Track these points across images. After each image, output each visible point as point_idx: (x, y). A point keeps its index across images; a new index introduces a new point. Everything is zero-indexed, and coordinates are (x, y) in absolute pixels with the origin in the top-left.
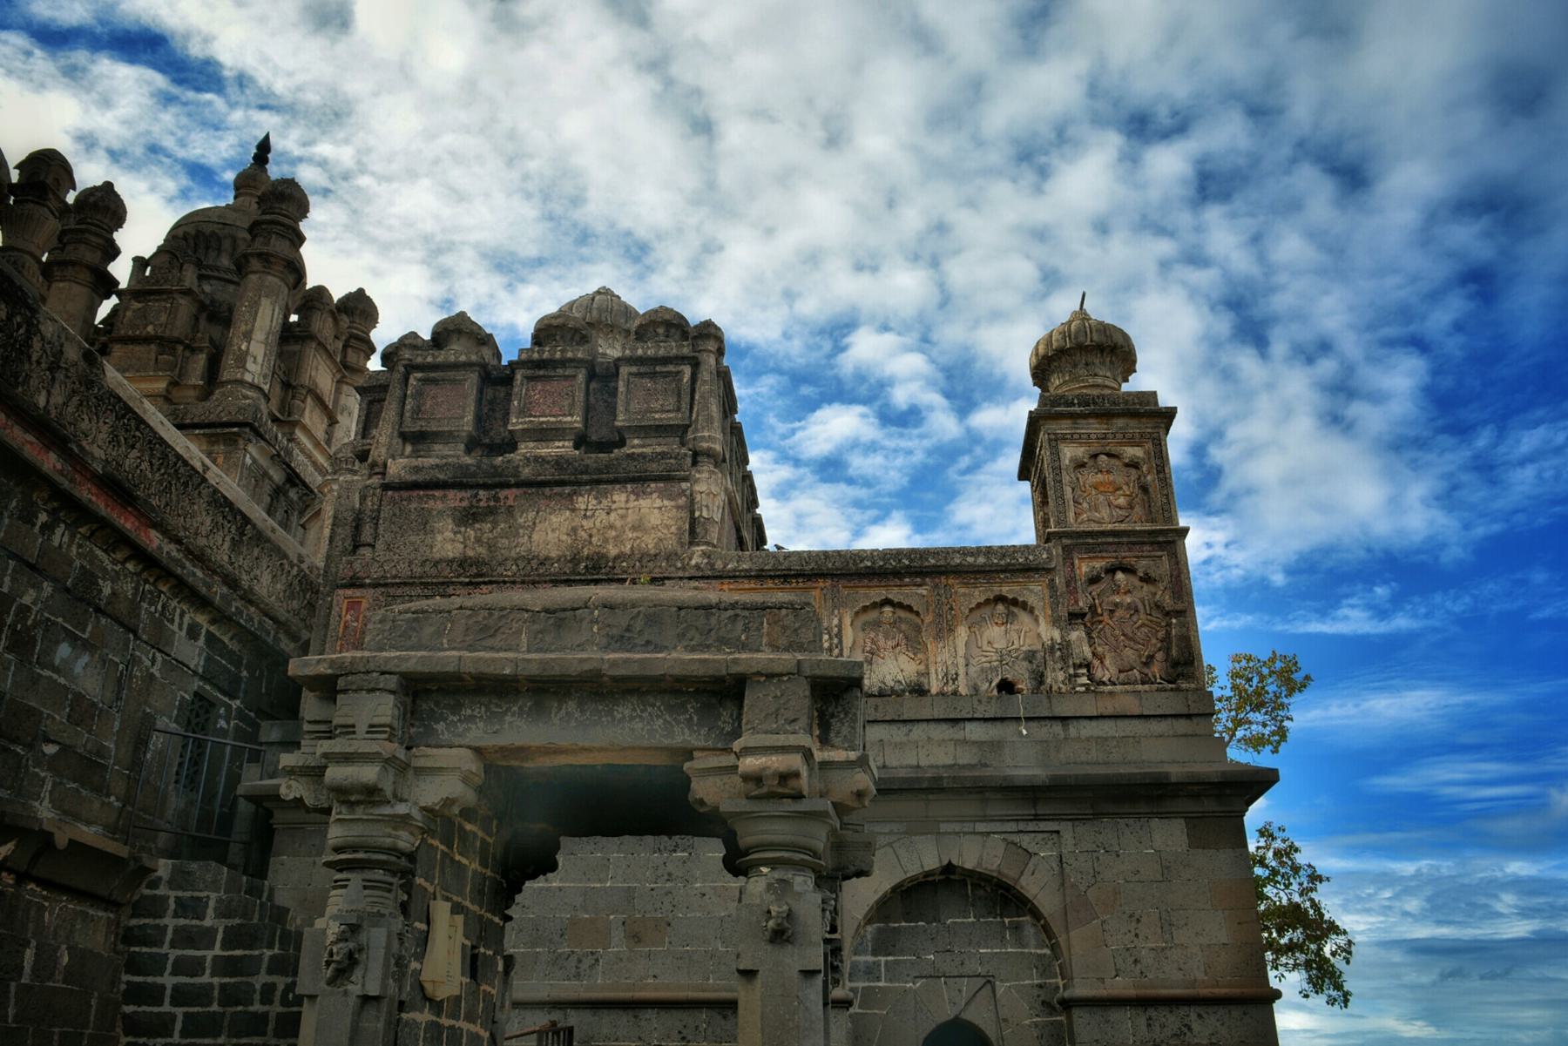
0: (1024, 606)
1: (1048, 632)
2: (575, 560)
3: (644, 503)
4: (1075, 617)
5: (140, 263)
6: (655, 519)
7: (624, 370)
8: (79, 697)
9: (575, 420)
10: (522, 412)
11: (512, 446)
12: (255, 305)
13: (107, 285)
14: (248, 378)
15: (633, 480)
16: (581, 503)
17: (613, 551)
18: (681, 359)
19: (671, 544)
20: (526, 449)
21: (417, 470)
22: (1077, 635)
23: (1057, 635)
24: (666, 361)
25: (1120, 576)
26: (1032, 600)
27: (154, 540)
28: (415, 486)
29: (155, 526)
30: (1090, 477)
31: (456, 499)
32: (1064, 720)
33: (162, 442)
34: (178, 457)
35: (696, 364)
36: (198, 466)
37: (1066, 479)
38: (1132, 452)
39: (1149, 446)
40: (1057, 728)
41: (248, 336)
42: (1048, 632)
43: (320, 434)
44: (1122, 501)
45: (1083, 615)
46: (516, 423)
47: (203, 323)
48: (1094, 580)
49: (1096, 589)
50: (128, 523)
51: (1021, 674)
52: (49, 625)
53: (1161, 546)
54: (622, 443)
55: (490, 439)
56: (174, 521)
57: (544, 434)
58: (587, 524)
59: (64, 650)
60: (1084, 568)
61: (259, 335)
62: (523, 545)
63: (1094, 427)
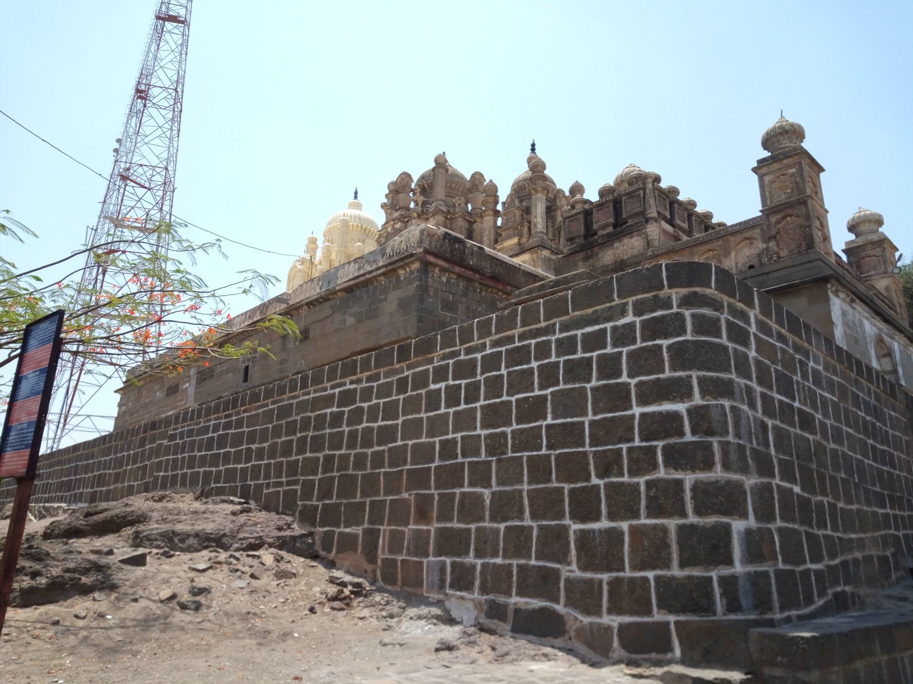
0: (754, 238)
1: (761, 245)
2: (616, 263)
3: (633, 240)
4: (771, 238)
5: (504, 204)
6: (636, 244)
7: (623, 198)
9: (611, 220)
10: (597, 222)
11: (596, 234)
12: (536, 205)
13: (497, 213)
17: (626, 258)
18: (639, 189)
19: (642, 250)
20: (600, 233)
22: (772, 244)
23: (764, 245)
24: (635, 191)
25: (789, 218)
26: (757, 236)
29: (508, 285)
30: (775, 185)
31: (582, 255)
32: (767, 274)
35: (644, 189)
37: (766, 189)
38: (794, 170)
39: (797, 167)
40: (765, 277)
41: (536, 217)
42: (761, 245)
43: (685, 226)
44: (789, 191)
45: (775, 237)
46: (595, 227)
48: (778, 222)
49: (779, 226)
53: (801, 204)
54: (626, 223)
55: (589, 232)
57: (604, 227)
60: (773, 219)
61: (539, 215)
62: (601, 263)
63: (776, 166)
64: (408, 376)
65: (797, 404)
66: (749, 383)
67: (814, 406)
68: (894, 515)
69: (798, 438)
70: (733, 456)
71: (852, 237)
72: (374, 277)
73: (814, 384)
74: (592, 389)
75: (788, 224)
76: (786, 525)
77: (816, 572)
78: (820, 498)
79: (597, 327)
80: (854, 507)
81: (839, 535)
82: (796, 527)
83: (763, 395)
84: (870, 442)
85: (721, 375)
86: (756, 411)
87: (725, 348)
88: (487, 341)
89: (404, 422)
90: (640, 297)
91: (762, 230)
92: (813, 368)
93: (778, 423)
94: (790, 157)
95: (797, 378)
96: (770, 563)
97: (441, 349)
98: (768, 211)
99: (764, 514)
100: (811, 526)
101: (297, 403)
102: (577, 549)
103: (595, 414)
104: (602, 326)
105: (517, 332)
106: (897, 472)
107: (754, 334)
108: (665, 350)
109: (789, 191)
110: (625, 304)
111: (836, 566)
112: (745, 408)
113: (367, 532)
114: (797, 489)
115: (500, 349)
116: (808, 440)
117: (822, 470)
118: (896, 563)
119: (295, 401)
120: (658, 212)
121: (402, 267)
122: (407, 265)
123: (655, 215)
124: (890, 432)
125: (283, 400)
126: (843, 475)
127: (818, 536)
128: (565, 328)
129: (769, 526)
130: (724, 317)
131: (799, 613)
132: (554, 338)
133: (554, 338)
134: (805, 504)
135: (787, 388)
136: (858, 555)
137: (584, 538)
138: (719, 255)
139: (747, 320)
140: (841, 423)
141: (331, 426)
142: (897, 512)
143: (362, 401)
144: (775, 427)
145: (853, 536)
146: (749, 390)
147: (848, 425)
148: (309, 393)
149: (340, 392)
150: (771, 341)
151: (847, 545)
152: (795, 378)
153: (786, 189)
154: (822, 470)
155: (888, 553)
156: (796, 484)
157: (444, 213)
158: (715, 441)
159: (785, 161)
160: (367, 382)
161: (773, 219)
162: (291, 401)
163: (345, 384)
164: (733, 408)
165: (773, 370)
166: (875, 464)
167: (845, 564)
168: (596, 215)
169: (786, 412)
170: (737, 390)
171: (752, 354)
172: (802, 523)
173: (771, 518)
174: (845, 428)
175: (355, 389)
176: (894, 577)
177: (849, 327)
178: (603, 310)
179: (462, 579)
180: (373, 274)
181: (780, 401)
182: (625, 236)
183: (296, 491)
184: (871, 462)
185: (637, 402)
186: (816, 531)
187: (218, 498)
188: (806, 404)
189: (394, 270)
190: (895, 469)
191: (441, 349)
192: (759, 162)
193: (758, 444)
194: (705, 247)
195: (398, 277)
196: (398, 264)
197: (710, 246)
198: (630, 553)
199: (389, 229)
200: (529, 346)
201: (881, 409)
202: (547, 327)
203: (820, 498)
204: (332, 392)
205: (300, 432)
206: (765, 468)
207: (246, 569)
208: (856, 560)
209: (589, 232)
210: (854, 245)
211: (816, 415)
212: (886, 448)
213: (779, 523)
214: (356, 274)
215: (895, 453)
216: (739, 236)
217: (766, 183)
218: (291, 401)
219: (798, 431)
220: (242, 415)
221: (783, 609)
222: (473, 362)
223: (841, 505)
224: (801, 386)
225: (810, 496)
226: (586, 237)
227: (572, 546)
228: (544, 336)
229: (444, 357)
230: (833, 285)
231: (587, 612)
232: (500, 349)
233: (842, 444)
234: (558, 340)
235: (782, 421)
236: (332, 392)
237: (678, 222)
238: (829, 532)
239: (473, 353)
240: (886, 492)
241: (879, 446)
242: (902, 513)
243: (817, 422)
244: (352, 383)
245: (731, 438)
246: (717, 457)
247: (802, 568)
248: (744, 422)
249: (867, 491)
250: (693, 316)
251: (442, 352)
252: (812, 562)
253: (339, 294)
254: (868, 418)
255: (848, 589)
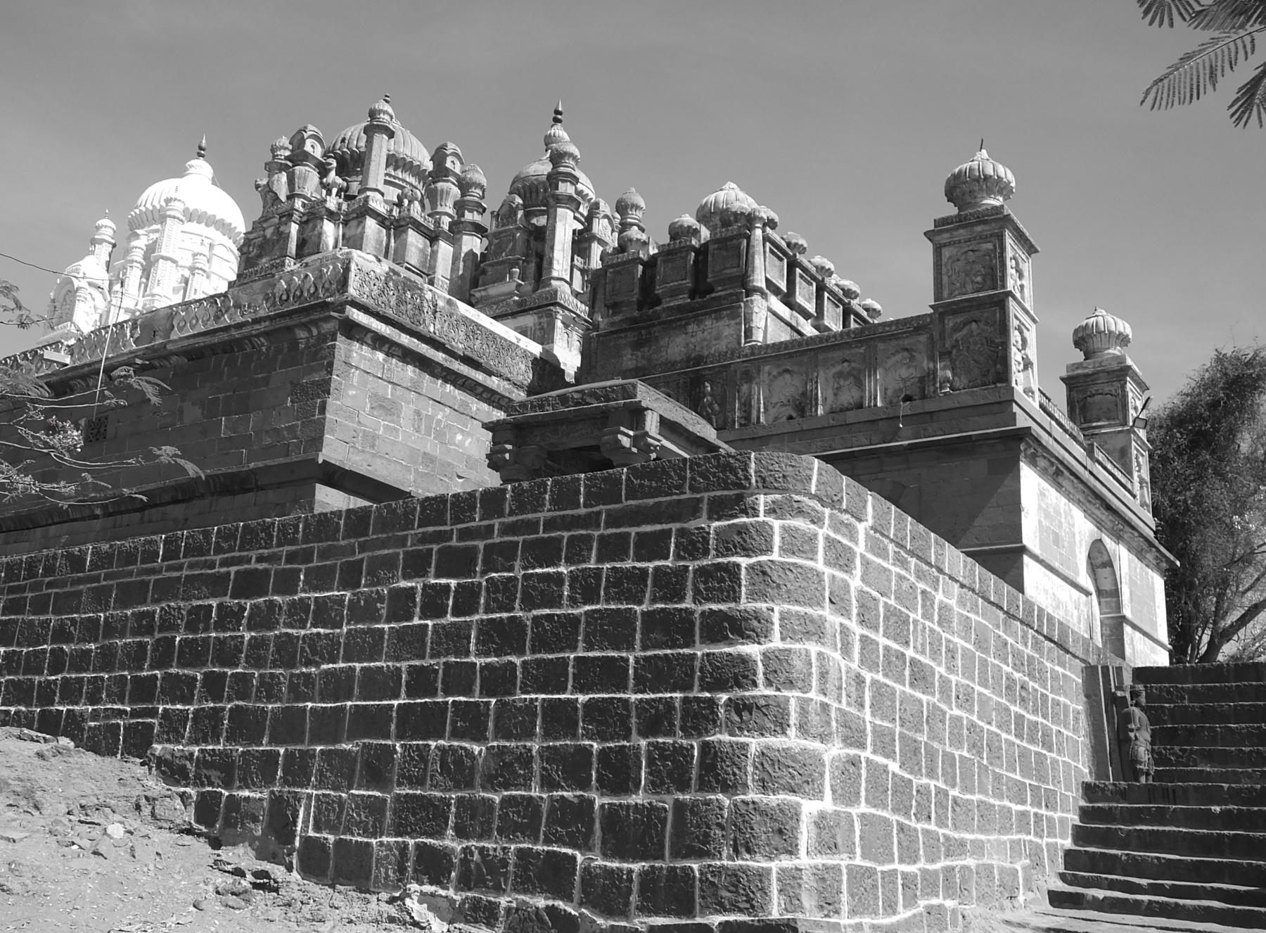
1: (926, 364)
7: (711, 247)
8: (469, 457)
9: (688, 283)
14: (555, 274)
15: (715, 312)
16: (690, 329)
21: (613, 324)
23: (931, 365)
24: (731, 238)
25: (974, 325)
27: (493, 382)
28: (612, 332)
31: (631, 337)
33: (492, 333)
34: (501, 338)
36: (515, 341)
37: (944, 270)
38: (990, 246)
43: (811, 307)
44: (979, 279)
46: (659, 290)
47: (532, 243)
48: (956, 329)
49: (959, 335)
50: (479, 376)
51: (914, 391)
52: (449, 427)
55: (648, 297)
56: (505, 371)
57: (674, 293)
58: (693, 340)
59: (459, 437)
64: (362, 560)
65: (910, 653)
66: (846, 622)
67: (935, 654)
68: (1036, 814)
69: (905, 698)
70: (814, 719)
71: (1079, 356)
72: (249, 338)
73: (940, 624)
74: (643, 613)
75: (971, 334)
76: (873, 811)
77: (905, 876)
78: (925, 781)
79: (658, 527)
80: (976, 797)
81: (947, 832)
82: (885, 814)
83: (864, 639)
84: (1015, 709)
85: (809, 610)
86: (852, 660)
87: (819, 575)
88: (496, 523)
89: (349, 631)
90: (718, 493)
91: (931, 338)
92: (941, 602)
93: (880, 677)
94: (985, 222)
95: (916, 615)
96: (845, 856)
97: (419, 526)
98: (943, 310)
99: (847, 794)
100: (907, 814)
101: (156, 581)
102: (602, 829)
103: (644, 648)
104: (665, 526)
105: (542, 516)
106: (1054, 755)
107: (862, 556)
108: (743, 572)
109: (979, 279)
110: (700, 500)
111: (936, 872)
112: (837, 655)
113: (276, 801)
114: (894, 767)
115: (516, 538)
116: (920, 702)
117: (936, 745)
118: (1027, 880)
119: (153, 578)
120: (767, 280)
121: (305, 326)
122: (315, 323)
123: (763, 285)
124: (1051, 696)
125: (130, 574)
126: (965, 754)
127: (916, 830)
128: (613, 520)
129: (849, 810)
130: (823, 532)
131: (875, 922)
132: (596, 533)
133: (596, 533)
134: (903, 786)
135: (898, 626)
136: (971, 862)
137: (611, 815)
138: (860, 371)
139: (853, 536)
140: (973, 680)
141: (220, 626)
142: (1043, 811)
143: (277, 592)
144: (874, 682)
145: (968, 836)
146: (845, 631)
147: (984, 683)
148: (180, 568)
149: (237, 572)
150: (885, 564)
151: (957, 848)
152: (912, 616)
153: (976, 275)
154: (936, 745)
155: (1018, 866)
156: (894, 760)
157: (379, 215)
158: (792, 695)
159: (979, 229)
160: (287, 562)
161: (950, 323)
162: (146, 578)
163: (249, 561)
164: (820, 654)
165: (881, 604)
166: (1018, 742)
167: (949, 870)
168: (661, 268)
169: (894, 662)
170: (829, 631)
171: (855, 583)
172: (895, 810)
173: (852, 799)
174: (977, 688)
175: (267, 571)
176: (1021, 898)
177: (1047, 515)
178: (669, 503)
179: (433, 866)
180: (245, 330)
181: (887, 648)
182: (709, 313)
183: (151, 726)
184: (1012, 738)
185: (701, 637)
186: (913, 823)
187: (16, 731)
188: (923, 652)
189: (289, 329)
190: (1051, 751)
191: (419, 526)
192: (940, 223)
193: (849, 704)
194: (838, 354)
195: (294, 343)
196: (296, 320)
197: (847, 353)
198: (672, 835)
199: (269, 233)
200: (560, 539)
201: (1040, 663)
202: (589, 515)
203: (925, 781)
204: (223, 570)
205: (160, 632)
206: (854, 737)
207: (86, 843)
208: (967, 868)
209: (648, 297)
210: (1080, 371)
211: (937, 669)
212: (1040, 720)
213: (863, 808)
214: (212, 325)
215: (1054, 728)
216: (894, 343)
217: (944, 260)
218: (146, 578)
219: (908, 689)
220: (45, 591)
221: (853, 912)
222: (471, 553)
223: (954, 793)
224: (920, 627)
225: (911, 777)
226: (641, 305)
227: (597, 825)
228: (582, 528)
229: (424, 539)
230: (1029, 446)
231: (609, 912)
232: (516, 538)
233: (971, 711)
234: (601, 537)
235: (886, 675)
236: (223, 570)
237: (800, 299)
238: (932, 827)
239: (472, 539)
240: (1028, 782)
241: (1027, 716)
242: (1050, 813)
243: (937, 677)
244: (260, 559)
245: (812, 695)
246: (793, 718)
247: (886, 868)
248: (833, 675)
249: (998, 777)
250: (783, 527)
251: (421, 530)
252: (901, 861)
253: (174, 358)
254: (1017, 675)
255: (950, 904)
